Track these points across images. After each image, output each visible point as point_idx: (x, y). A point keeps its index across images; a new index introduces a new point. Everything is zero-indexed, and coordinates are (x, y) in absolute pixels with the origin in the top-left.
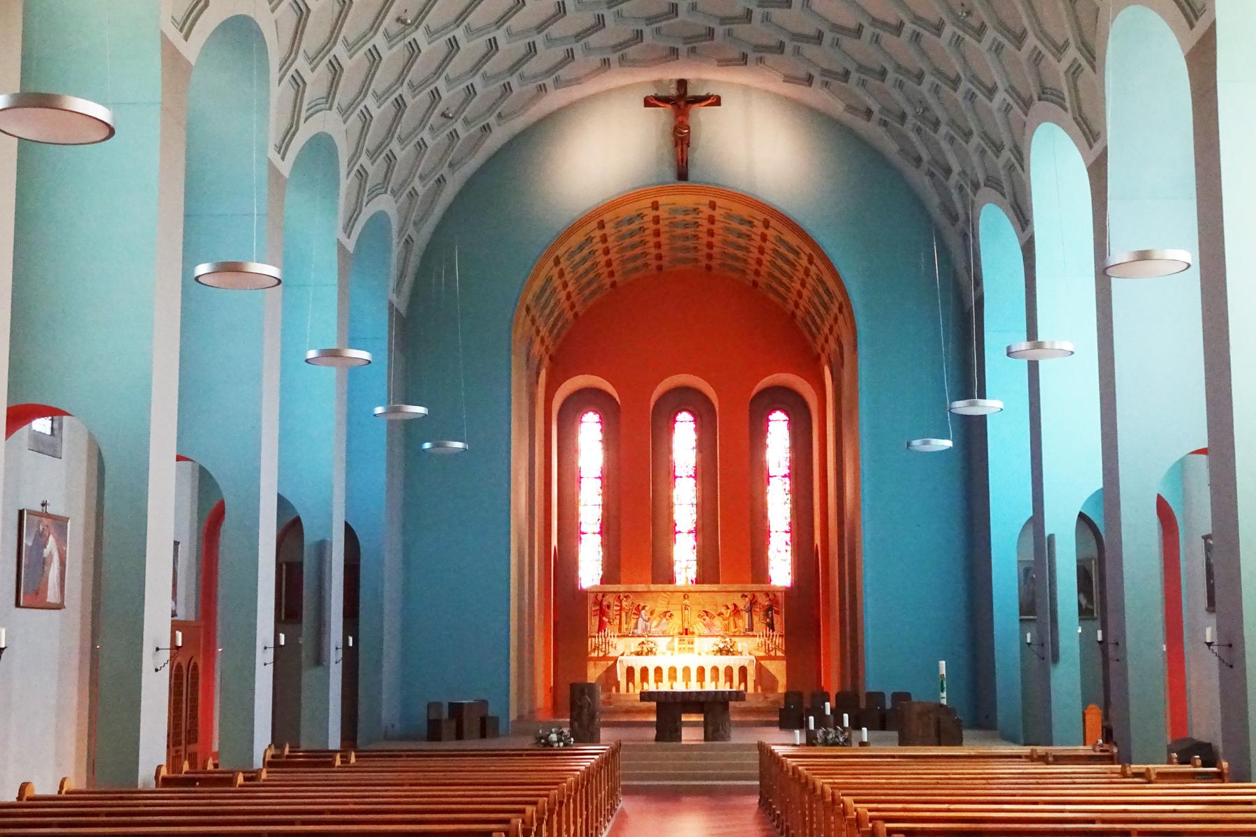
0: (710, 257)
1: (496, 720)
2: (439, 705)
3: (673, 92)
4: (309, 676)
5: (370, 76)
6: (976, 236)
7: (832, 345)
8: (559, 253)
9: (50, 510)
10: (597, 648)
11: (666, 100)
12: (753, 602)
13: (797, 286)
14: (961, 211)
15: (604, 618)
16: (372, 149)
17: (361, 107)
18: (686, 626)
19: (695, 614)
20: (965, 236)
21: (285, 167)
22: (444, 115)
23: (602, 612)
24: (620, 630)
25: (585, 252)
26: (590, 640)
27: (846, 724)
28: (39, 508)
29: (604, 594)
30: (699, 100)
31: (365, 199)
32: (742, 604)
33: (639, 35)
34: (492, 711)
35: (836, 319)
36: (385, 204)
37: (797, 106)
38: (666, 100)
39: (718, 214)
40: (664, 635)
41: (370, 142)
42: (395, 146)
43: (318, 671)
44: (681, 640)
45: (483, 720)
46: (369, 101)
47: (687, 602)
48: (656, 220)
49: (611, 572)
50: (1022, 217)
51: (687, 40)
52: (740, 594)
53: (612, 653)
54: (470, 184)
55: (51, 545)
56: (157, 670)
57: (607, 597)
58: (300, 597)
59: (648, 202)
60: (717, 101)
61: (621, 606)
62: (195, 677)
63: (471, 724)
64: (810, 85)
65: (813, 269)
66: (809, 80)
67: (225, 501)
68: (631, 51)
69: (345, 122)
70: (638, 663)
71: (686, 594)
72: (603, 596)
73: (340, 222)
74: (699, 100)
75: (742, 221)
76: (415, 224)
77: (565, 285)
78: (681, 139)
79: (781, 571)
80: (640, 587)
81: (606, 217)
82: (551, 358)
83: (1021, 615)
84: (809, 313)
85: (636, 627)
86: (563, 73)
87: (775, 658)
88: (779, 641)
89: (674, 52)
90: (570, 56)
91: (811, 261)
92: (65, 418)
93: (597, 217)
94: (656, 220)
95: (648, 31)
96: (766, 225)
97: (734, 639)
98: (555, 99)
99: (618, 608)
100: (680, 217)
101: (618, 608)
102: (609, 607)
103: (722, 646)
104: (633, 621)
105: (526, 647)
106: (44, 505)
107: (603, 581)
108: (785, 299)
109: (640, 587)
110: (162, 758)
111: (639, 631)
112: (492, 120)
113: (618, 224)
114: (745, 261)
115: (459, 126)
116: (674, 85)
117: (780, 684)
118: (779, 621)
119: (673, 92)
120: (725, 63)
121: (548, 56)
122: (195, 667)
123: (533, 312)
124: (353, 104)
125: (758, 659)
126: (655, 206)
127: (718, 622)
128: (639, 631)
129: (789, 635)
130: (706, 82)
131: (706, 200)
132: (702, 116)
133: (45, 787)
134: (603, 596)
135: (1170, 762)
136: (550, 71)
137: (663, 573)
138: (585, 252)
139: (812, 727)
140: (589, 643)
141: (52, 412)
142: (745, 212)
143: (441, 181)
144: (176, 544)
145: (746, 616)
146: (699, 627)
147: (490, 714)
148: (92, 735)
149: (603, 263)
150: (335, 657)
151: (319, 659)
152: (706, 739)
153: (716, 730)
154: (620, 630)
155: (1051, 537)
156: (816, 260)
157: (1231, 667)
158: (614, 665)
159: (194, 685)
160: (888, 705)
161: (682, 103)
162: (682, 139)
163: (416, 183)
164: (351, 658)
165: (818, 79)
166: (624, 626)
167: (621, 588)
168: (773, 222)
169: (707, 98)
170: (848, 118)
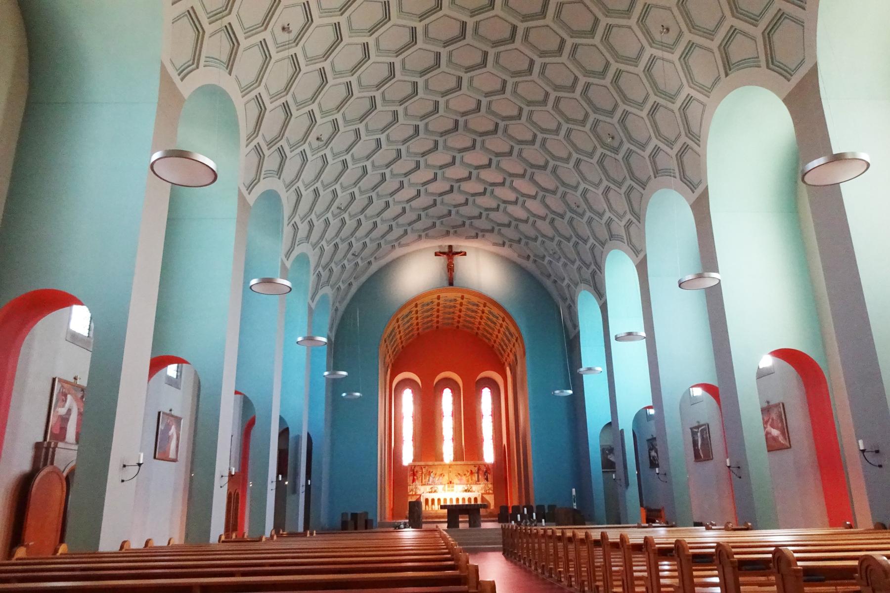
0: (459, 322)
1: (372, 521)
2: (347, 514)
3: (446, 250)
4: (290, 499)
5: (325, 231)
6: (576, 307)
7: (512, 356)
8: (399, 316)
9: (173, 413)
10: (412, 490)
11: (444, 253)
12: (479, 469)
13: (496, 333)
14: (568, 296)
16: (324, 265)
17: (320, 245)
20: (570, 307)
21: (288, 264)
22: (353, 255)
23: (414, 474)
24: (422, 482)
25: (409, 317)
27: (535, 518)
28: (168, 411)
29: (415, 466)
30: (457, 253)
31: (320, 287)
32: (475, 470)
33: (434, 225)
34: (370, 517)
35: (514, 345)
36: (327, 291)
37: (497, 255)
38: (444, 253)
39: (464, 301)
40: (441, 484)
41: (324, 261)
42: (333, 265)
43: (293, 497)
44: (448, 487)
45: (366, 521)
46: (324, 243)
47: (450, 469)
48: (438, 304)
49: (417, 456)
50: (600, 293)
51: (453, 227)
53: (419, 493)
54: (360, 290)
55: (173, 430)
56: (221, 487)
58: (286, 465)
59: (436, 296)
60: (465, 254)
62: (237, 499)
63: (361, 522)
64: (504, 246)
65: (504, 324)
66: (504, 244)
67: (256, 419)
68: (431, 232)
69: (314, 250)
70: (430, 496)
71: (450, 466)
73: (310, 295)
74: (457, 253)
75: (474, 305)
76: (339, 302)
77: (400, 332)
78: (450, 269)
79: (489, 456)
80: (430, 463)
81: (418, 302)
82: (392, 365)
83: (603, 469)
84: (500, 345)
85: (429, 481)
86: (403, 241)
87: (489, 494)
88: (490, 486)
89: (448, 233)
90: (406, 232)
91: (503, 320)
92: (184, 365)
93: (415, 301)
94: (438, 304)
95: (438, 223)
96: (485, 305)
98: (399, 252)
100: (448, 303)
102: (417, 472)
103: (466, 488)
104: (427, 478)
105: (383, 488)
106: (171, 410)
107: (414, 460)
108: (489, 340)
109: (430, 463)
110: (222, 530)
111: (430, 483)
112: (372, 259)
113: (423, 306)
114: (473, 323)
115: (359, 260)
116: (447, 247)
118: (490, 477)
119: (446, 250)
120: (468, 238)
121: (397, 232)
122: (238, 494)
123: (400, 322)
124: (318, 243)
125: (482, 494)
126: (439, 298)
127: (464, 478)
128: (430, 483)
129: (494, 484)
130: (460, 246)
131: (460, 295)
132: (458, 259)
133: (160, 541)
136: (397, 240)
137: (439, 457)
138: (409, 317)
139: (519, 519)
141: (179, 361)
142: (475, 300)
143: (350, 284)
144: (232, 436)
145: (476, 475)
146: (456, 480)
147: (369, 518)
148: (187, 525)
149: (415, 324)
150: (302, 489)
151: (295, 490)
152: (470, 526)
153: (475, 522)
154: (422, 482)
155: (622, 430)
156: (506, 319)
157: (740, 478)
158: (420, 498)
159: (237, 502)
160: (547, 511)
161: (451, 254)
162: (451, 269)
163: (340, 284)
164: (308, 488)
165: (507, 243)
166: (424, 481)
167: (422, 463)
168: (488, 304)
169: (461, 252)
170: (520, 261)
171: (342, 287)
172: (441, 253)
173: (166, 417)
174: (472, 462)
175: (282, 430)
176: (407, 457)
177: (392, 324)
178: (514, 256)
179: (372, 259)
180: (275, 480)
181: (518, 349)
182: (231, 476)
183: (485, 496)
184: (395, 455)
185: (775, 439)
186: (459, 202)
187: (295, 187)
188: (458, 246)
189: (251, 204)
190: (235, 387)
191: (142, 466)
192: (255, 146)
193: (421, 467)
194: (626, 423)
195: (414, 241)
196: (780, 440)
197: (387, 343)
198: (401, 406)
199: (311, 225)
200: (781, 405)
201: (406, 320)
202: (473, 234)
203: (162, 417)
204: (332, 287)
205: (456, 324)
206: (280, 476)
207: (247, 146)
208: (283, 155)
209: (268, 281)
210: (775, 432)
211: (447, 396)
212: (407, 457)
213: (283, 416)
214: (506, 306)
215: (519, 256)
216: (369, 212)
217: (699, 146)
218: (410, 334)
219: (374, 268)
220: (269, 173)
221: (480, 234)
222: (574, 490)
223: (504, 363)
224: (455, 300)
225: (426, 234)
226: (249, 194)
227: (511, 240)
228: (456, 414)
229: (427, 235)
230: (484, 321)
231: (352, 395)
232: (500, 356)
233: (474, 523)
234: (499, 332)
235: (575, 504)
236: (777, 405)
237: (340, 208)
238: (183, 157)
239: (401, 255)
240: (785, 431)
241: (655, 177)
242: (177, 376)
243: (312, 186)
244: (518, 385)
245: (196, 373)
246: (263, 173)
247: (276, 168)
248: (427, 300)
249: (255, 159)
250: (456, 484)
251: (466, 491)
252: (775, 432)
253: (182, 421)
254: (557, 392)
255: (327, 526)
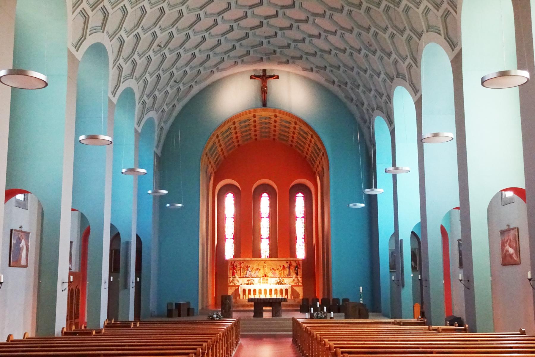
1: (193, 309)
3: (261, 74)
4: (122, 293)
8: (218, 133)
9: (23, 229)
12: (290, 265)
15: (234, 271)
18: (265, 274)
19: (268, 269)
20: (369, 128)
23: (234, 268)
24: (240, 275)
26: (229, 279)
27: (325, 310)
33: (248, 52)
35: (321, 159)
36: (152, 114)
39: (278, 119)
40: (257, 277)
49: (237, 254)
50: (390, 121)
52: (285, 262)
53: (238, 284)
55: (23, 243)
56: (63, 291)
57: (236, 263)
60: (277, 77)
61: (241, 266)
63: (184, 310)
68: (245, 59)
70: (247, 287)
71: (265, 262)
72: (234, 262)
77: (220, 146)
78: (264, 91)
79: (301, 253)
80: (248, 259)
81: (236, 120)
82: (215, 172)
85: (246, 274)
86: (221, 66)
87: (299, 286)
88: (300, 279)
90: (223, 59)
91: (312, 137)
92: (29, 194)
93: (232, 120)
94: (255, 121)
96: (296, 123)
97: (283, 278)
98: (217, 76)
99: (240, 267)
101: (240, 267)
102: (236, 266)
103: (278, 281)
104: (245, 272)
106: (20, 227)
109: (248, 259)
113: (240, 123)
115: (181, 85)
116: (261, 71)
117: (300, 295)
119: (261, 73)
120: (280, 63)
122: (79, 289)
125: (292, 286)
127: (277, 272)
128: (248, 276)
130: (274, 70)
131: (273, 114)
132: (272, 83)
133: (18, 336)
134: (234, 262)
135: (446, 325)
136: (215, 66)
137: (257, 254)
139: (312, 311)
140: (229, 280)
143: (174, 106)
145: (288, 270)
146: (270, 274)
147: (191, 307)
151: (126, 286)
152: (273, 316)
154: (240, 275)
155: (401, 240)
156: (314, 137)
162: (264, 91)
166: (242, 274)
169: (274, 76)
170: (326, 84)
171: (166, 109)
172: (255, 76)
173: (17, 233)
174: (284, 259)
175: (113, 235)
176: (229, 253)
177: (213, 140)
178: (322, 81)
179: (193, 83)
180: (107, 280)
181: (324, 163)
182: (70, 282)
183: (295, 288)
184: (219, 251)
185: (511, 256)
186: (269, 34)
187: (118, 35)
188: (272, 70)
189: (80, 60)
190: (72, 206)
191: (3, 284)
192: (81, 11)
193: (240, 263)
194: (405, 236)
195: (232, 66)
196: (514, 257)
197: (208, 156)
198: (224, 208)
199: (134, 64)
200: (516, 229)
201: (225, 135)
202: (284, 60)
203: (14, 234)
204: (157, 110)
205: (273, 137)
206: (112, 278)
207: (73, 12)
208: (106, 12)
209: (93, 137)
210: (511, 251)
211: (265, 202)
212: (229, 253)
213: (113, 223)
214: (313, 125)
215: (326, 80)
216: (187, 45)
217: (456, 12)
218: (231, 146)
219: (196, 89)
220: (95, 30)
221: (290, 61)
222: (361, 288)
223: (315, 172)
224: (270, 118)
225: (241, 60)
226: (77, 51)
227: (317, 67)
228: (272, 216)
229: (242, 61)
230: (296, 136)
231: (174, 205)
232: (312, 166)
233: (276, 313)
234: (309, 146)
235: (362, 299)
236: (514, 229)
237: (160, 46)
238: (22, 75)
239: (219, 78)
240: (517, 250)
241: (427, 32)
242: (24, 198)
243: (132, 33)
244: (324, 194)
245: (39, 204)
246: (88, 30)
247: (100, 23)
248: (244, 118)
249: (81, 20)
250: (270, 277)
251: (278, 283)
252: (511, 251)
253: (30, 234)
254: (351, 205)
255: (156, 313)
